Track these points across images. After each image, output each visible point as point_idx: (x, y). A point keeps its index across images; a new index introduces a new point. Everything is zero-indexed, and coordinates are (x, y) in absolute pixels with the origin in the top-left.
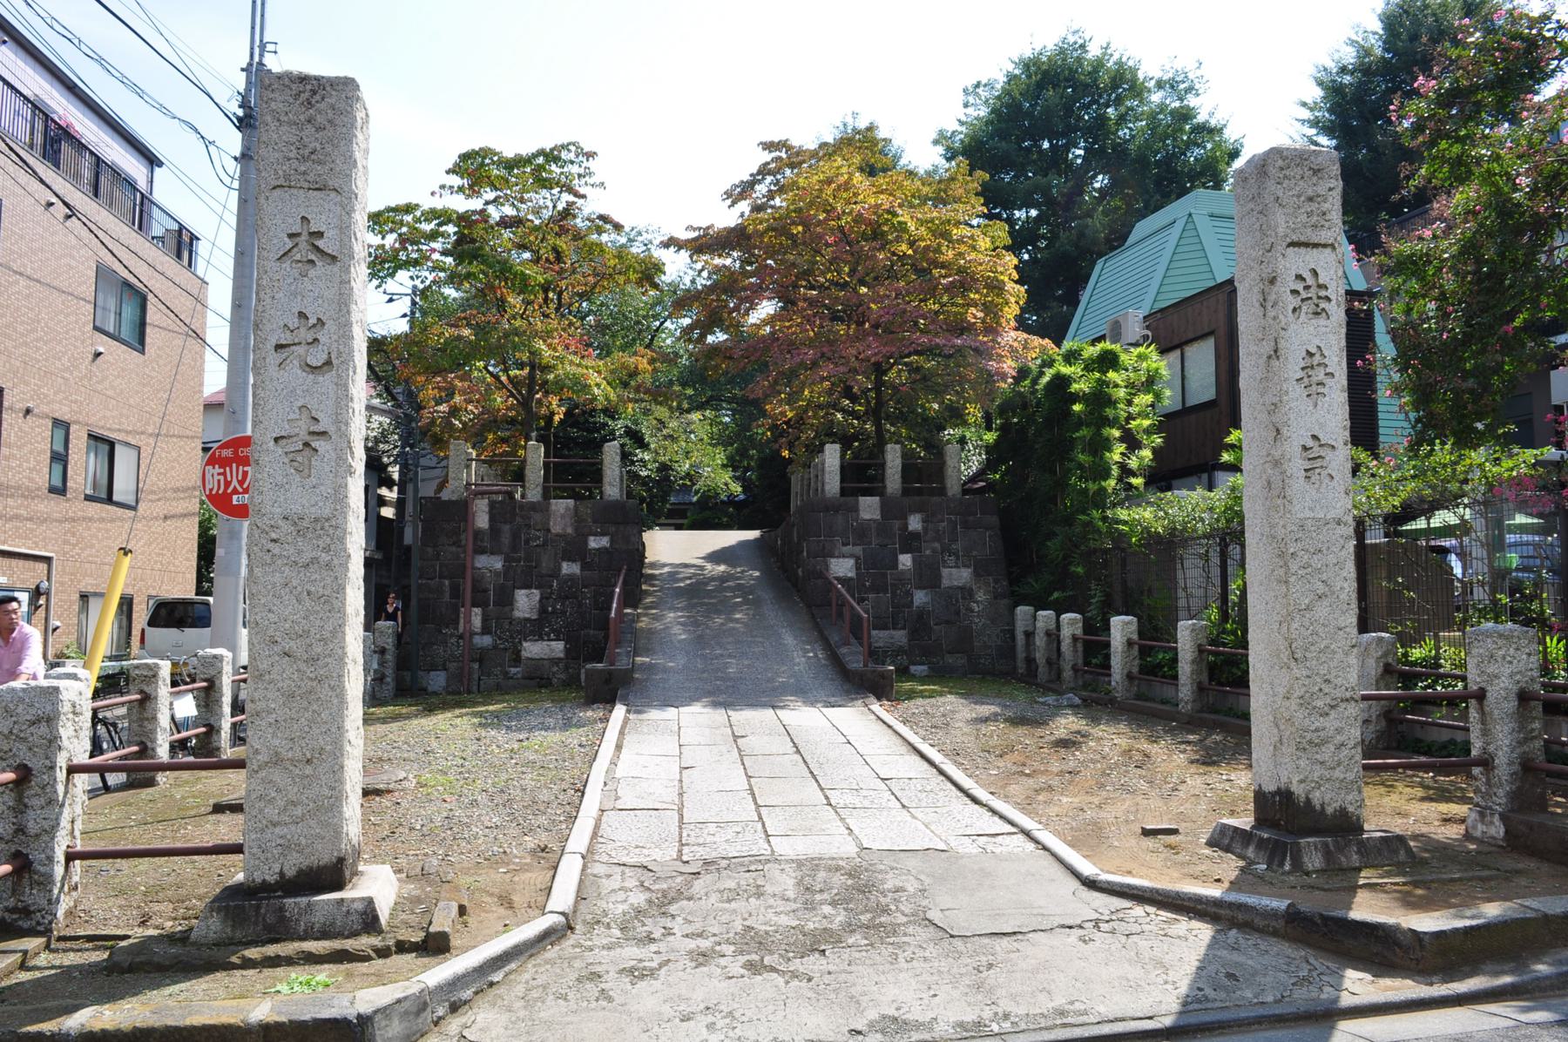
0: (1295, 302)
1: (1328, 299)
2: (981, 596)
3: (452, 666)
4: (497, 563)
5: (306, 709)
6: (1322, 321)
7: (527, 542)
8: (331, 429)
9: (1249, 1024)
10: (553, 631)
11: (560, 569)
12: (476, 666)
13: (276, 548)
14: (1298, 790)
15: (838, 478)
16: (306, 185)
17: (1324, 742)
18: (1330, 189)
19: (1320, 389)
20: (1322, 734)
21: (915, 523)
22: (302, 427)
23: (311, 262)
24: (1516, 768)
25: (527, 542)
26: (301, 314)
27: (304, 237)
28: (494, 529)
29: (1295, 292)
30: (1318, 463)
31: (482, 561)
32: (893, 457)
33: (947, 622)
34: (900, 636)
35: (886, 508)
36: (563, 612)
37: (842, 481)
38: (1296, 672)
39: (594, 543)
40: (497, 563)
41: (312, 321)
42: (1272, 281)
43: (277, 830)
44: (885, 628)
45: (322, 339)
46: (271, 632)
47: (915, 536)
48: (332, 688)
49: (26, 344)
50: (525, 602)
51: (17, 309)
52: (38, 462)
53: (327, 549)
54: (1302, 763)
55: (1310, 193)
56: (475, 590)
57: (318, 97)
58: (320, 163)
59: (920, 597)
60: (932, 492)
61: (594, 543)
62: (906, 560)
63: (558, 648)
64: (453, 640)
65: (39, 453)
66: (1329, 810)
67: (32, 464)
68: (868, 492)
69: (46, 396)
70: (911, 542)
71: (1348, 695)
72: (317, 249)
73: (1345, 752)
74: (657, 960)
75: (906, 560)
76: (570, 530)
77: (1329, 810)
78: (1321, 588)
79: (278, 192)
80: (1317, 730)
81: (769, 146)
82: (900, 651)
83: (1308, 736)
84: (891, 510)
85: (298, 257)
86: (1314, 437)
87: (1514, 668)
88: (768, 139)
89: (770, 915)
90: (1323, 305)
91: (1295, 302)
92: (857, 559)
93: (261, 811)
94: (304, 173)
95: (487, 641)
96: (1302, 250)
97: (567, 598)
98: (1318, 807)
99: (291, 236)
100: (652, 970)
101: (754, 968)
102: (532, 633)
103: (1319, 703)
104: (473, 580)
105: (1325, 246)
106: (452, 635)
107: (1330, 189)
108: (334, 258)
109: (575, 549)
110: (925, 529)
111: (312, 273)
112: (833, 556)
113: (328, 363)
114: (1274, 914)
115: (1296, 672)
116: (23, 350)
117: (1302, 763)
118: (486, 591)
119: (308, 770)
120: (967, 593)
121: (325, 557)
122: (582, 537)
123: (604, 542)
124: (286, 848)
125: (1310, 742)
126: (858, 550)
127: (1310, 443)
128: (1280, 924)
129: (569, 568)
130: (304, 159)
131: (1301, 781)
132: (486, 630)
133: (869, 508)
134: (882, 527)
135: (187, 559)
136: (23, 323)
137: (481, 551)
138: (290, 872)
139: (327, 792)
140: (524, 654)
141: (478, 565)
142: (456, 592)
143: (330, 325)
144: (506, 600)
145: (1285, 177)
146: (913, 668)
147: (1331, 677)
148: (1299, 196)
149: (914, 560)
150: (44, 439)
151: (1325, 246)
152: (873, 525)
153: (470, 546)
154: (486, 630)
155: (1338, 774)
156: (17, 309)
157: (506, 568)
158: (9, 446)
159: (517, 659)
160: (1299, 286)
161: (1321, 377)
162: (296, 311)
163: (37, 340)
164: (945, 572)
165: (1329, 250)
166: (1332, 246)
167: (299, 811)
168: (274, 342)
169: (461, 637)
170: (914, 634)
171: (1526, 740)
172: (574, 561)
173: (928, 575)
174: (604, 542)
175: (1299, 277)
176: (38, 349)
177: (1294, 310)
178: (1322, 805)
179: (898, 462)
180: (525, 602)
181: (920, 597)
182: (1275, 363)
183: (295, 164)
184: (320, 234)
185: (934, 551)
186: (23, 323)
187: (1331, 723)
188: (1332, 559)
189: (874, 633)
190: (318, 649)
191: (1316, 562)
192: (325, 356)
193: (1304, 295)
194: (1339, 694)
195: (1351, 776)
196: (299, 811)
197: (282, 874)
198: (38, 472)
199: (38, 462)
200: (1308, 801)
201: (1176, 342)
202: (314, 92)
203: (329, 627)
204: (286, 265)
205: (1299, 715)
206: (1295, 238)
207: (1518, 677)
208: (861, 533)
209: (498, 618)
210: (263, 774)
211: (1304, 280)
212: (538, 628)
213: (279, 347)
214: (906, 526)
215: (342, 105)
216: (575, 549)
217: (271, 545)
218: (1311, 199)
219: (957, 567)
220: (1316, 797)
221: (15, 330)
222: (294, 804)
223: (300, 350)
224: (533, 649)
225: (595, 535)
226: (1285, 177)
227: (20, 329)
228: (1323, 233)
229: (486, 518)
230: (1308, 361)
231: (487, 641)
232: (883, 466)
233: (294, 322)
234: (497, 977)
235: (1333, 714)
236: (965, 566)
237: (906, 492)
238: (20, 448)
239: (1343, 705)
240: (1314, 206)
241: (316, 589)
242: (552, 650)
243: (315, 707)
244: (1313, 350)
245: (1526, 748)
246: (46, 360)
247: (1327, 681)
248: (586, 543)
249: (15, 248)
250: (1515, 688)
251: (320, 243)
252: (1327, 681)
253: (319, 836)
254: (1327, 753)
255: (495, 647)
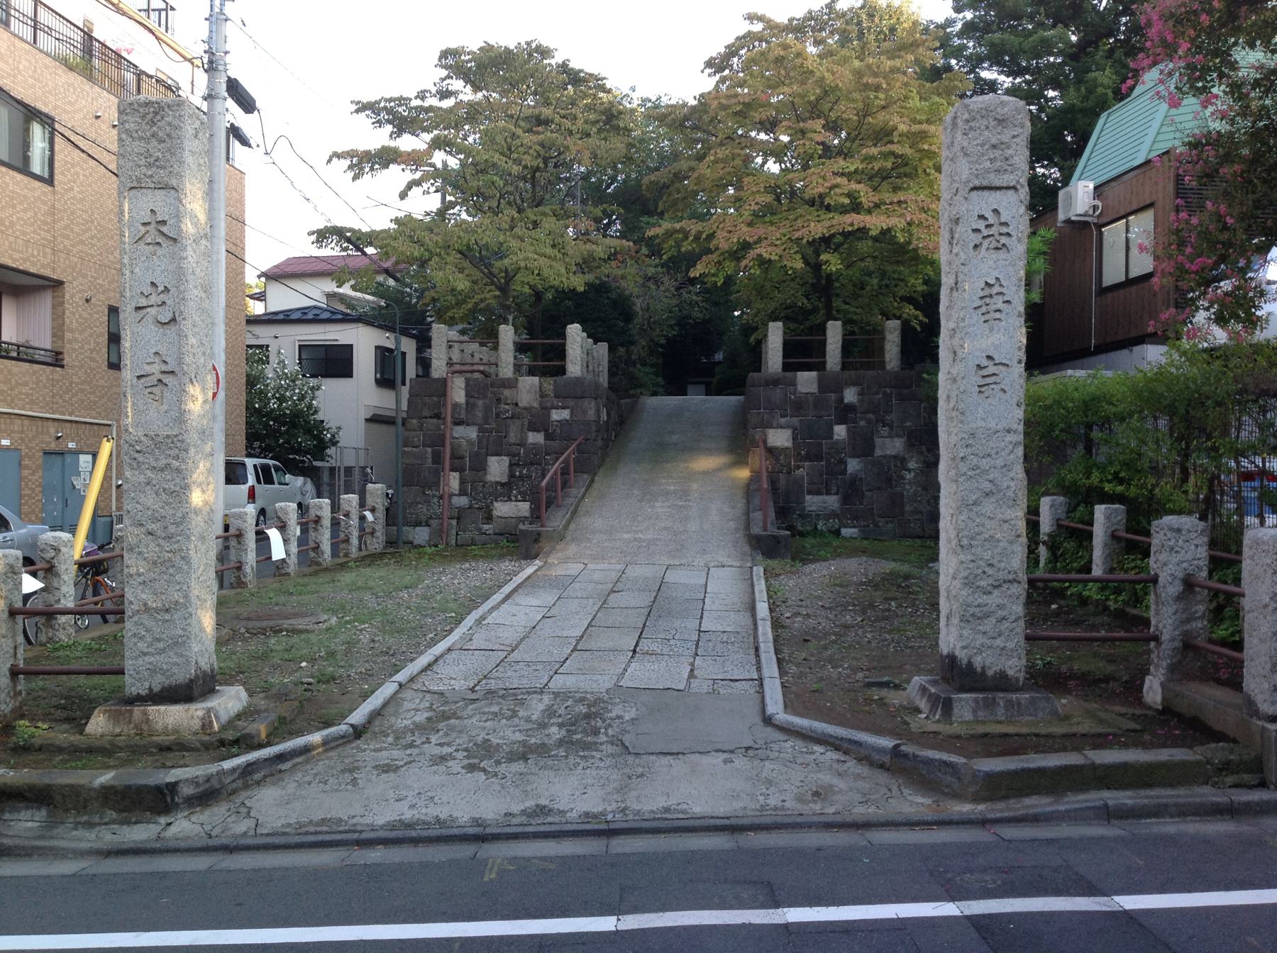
0: (976, 238)
1: (1008, 235)
2: (912, 464)
3: (434, 523)
4: (472, 433)
5: (165, 573)
6: (1002, 254)
7: (498, 415)
8: (177, 370)
9: (810, 827)
10: (520, 493)
11: (527, 437)
12: (454, 522)
13: (140, 458)
14: (962, 655)
15: (780, 354)
16: (152, 185)
17: (987, 615)
18: (1014, 137)
19: (997, 315)
20: (985, 609)
21: (850, 395)
22: (156, 368)
23: (158, 244)
24: (1177, 644)
25: (498, 415)
26: (152, 283)
27: (153, 225)
28: (470, 406)
29: (976, 231)
30: (992, 379)
31: (459, 431)
32: (834, 333)
33: (879, 489)
34: (833, 501)
35: (824, 386)
36: (529, 477)
37: (784, 356)
38: (962, 557)
39: (556, 415)
40: (472, 433)
41: (161, 288)
42: (957, 221)
43: (146, 658)
44: (818, 493)
45: (168, 302)
46: (138, 517)
47: (851, 408)
48: (183, 558)
49: (82, 242)
50: (497, 468)
51: (73, 213)
52: (98, 344)
53: (177, 458)
54: (965, 633)
55: (994, 141)
56: (453, 457)
57: (159, 117)
58: (161, 168)
59: (853, 465)
60: (869, 366)
61: (556, 415)
62: (840, 431)
63: (524, 508)
64: (435, 500)
65: (98, 336)
66: (990, 673)
67: (92, 345)
68: (808, 367)
69: (101, 286)
70: (845, 413)
71: (1011, 577)
72: (162, 233)
73: (1006, 625)
74: (407, 759)
75: (840, 431)
76: (535, 405)
77: (990, 673)
78: (987, 486)
79: (133, 192)
80: (979, 606)
81: (751, 18)
82: (834, 515)
83: (972, 610)
84: (830, 385)
85: (149, 240)
86: (989, 357)
87: (1179, 557)
88: (752, 10)
89: (509, 733)
90: (1004, 240)
91: (976, 238)
92: (795, 429)
93: (135, 644)
94: (151, 176)
95: (463, 501)
96: (986, 193)
97: (532, 464)
98: (979, 670)
99: (144, 224)
100: (398, 768)
101: (471, 768)
102: (502, 495)
103: (983, 583)
104: (452, 449)
105: (1008, 188)
106: (434, 496)
107: (1014, 137)
108: (175, 240)
109: (538, 421)
110: (861, 401)
111: (160, 252)
112: (772, 427)
113: (173, 320)
114: (880, 750)
115: (962, 557)
116: (80, 247)
117: (965, 633)
118: (462, 458)
119: (167, 617)
120: (900, 460)
121: (175, 463)
122: (546, 410)
123: (565, 414)
124: (153, 671)
125: (973, 615)
126: (795, 420)
127: (985, 362)
128: (886, 759)
129: (536, 438)
130: (150, 165)
131: (964, 648)
132: (463, 492)
133: (807, 381)
134: (817, 401)
135: (237, 423)
136: (78, 224)
137: (458, 423)
138: (157, 689)
139: (180, 632)
140: (495, 513)
141: (456, 435)
142: (437, 458)
143: (173, 290)
144: (479, 466)
145: (971, 128)
146: (844, 531)
147: (995, 562)
148: (982, 145)
149: (848, 430)
150: (101, 323)
151: (1008, 188)
152: (811, 399)
153: (449, 419)
154: (463, 492)
155: (999, 642)
156: (73, 213)
157: (480, 439)
158: (72, 331)
159: (489, 518)
160: (981, 225)
161: (1000, 305)
162: (148, 281)
163: (92, 238)
164: (878, 441)
165: (1011, 192)
166: (1014, 188)
167: (161, 645)
168: (134, 305)
169: (441, 497)
170: (846, 500)
171: (1188, 620)
172: (539, 431)
173: (863, 445)
174: (565, 414)
175: (982, 217)
176: (93, 245)
177: (976, 246)
178: (983, 668)
179: (839, 338)
180: (497, 468)
181: (853, 465)
182: (955, 294)
183: (144, 170)
184: (164, 222)
185: (869, 422)
186: (78, 224)
187: (995, 599)
188: (1000, 462)
189: (808, 498)
190: (172, 529)
191: (985, 464)
192: (171, 315)
193: (986, 232)
194: (1002, 575)
195: (1011, 645)
196: (161, 645)
197: (150, 689)
198: (98, 352)
199: (98, 344)
200: (970, 664)
201: (1122, 213)
202: (156, 113)
203: (179, 514)
204: (142, 246)
205: (964, 593)
206: (977, 183)
207: (1185, 565)
208: (799, 406)
209: (473, 482)
210: (136, 618)
211: (986, 219)
212: (506, 490)
213: (138, 308)
214: (842, 398)
215: (175, 122)
216: (538, 421)
217: (137, 455)
218: (994, 147)
219: (890, 436)
220: (978, 662)
221: (72, 231)
222: (159, 640)
223: (152, 311)
224: (503, 509)
225: (557, 408)
226: (971, 128)
227: (76, 229)
228: (1006, 177)
229: (463, 393)
230: (987, 292)
231: (463, 501)
232: (823, 343)
233: (148, 289)
234: (284, 767)
235: (996, 592)
236: (898, 436)
237: (845, 366)
238: (81, 332)
239: (1006, 586)
240: (997, 153)
241: (171, 486)
242: (519, 510)
243: (171, 571)
244: (992, 282)
245: (1188, 627)
246: (101, 254)
247: (991, 565)
248: (549, 416)
249: (69, 159)
250: (1181, 575)
251: (164, 229)
252: (991, 565)
253: (176, 664)
254: (988, 625)
255: (471, 507)
